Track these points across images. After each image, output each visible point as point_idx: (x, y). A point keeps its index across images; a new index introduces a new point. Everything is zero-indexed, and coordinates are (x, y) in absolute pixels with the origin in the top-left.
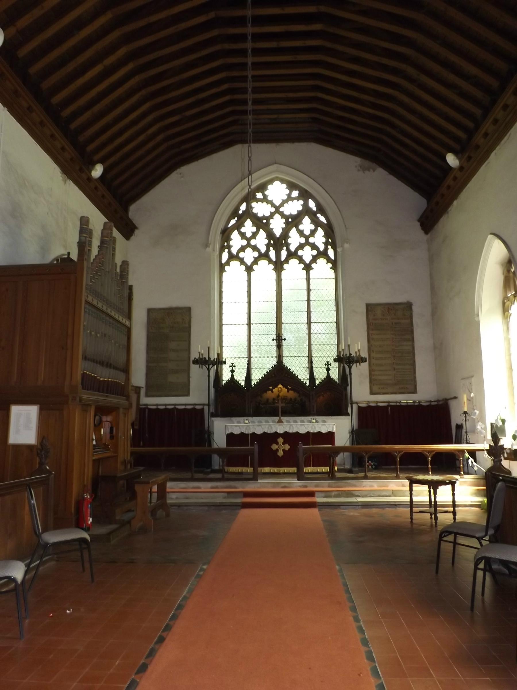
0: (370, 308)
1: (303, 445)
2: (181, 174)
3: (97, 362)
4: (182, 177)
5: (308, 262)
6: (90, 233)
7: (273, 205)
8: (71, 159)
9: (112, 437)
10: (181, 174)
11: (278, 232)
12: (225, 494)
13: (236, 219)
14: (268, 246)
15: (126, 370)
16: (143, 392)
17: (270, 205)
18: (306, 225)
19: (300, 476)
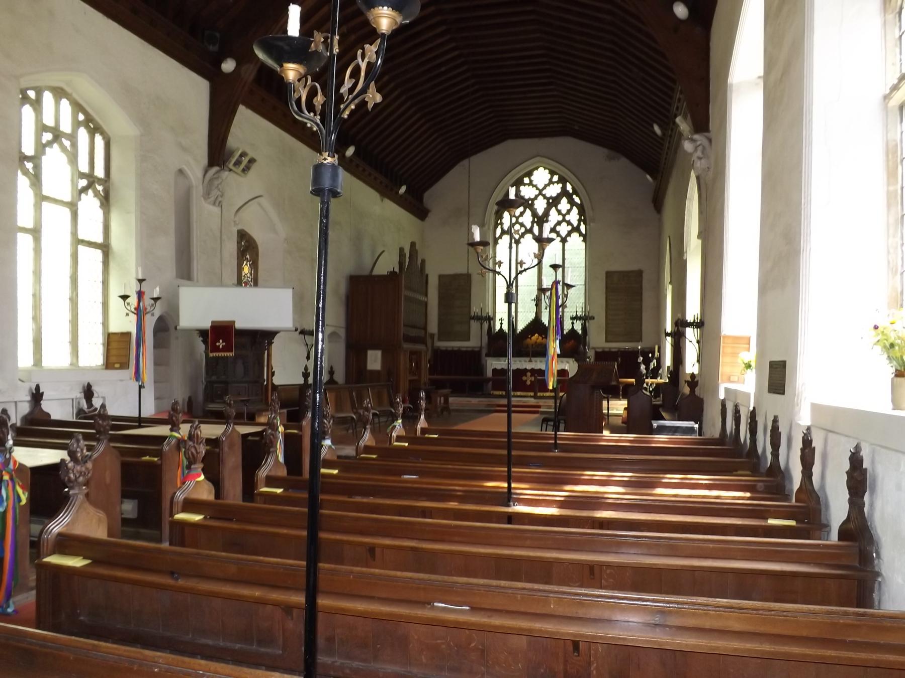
0: (609, 274)
1: (539, 376)
5: (564, 236)
7: (537, 189)
11: (540, 212)
14: (533, 222)
15: (425, 328)
17: (535, 188)
18: (564, 205)
19: (535, 397)
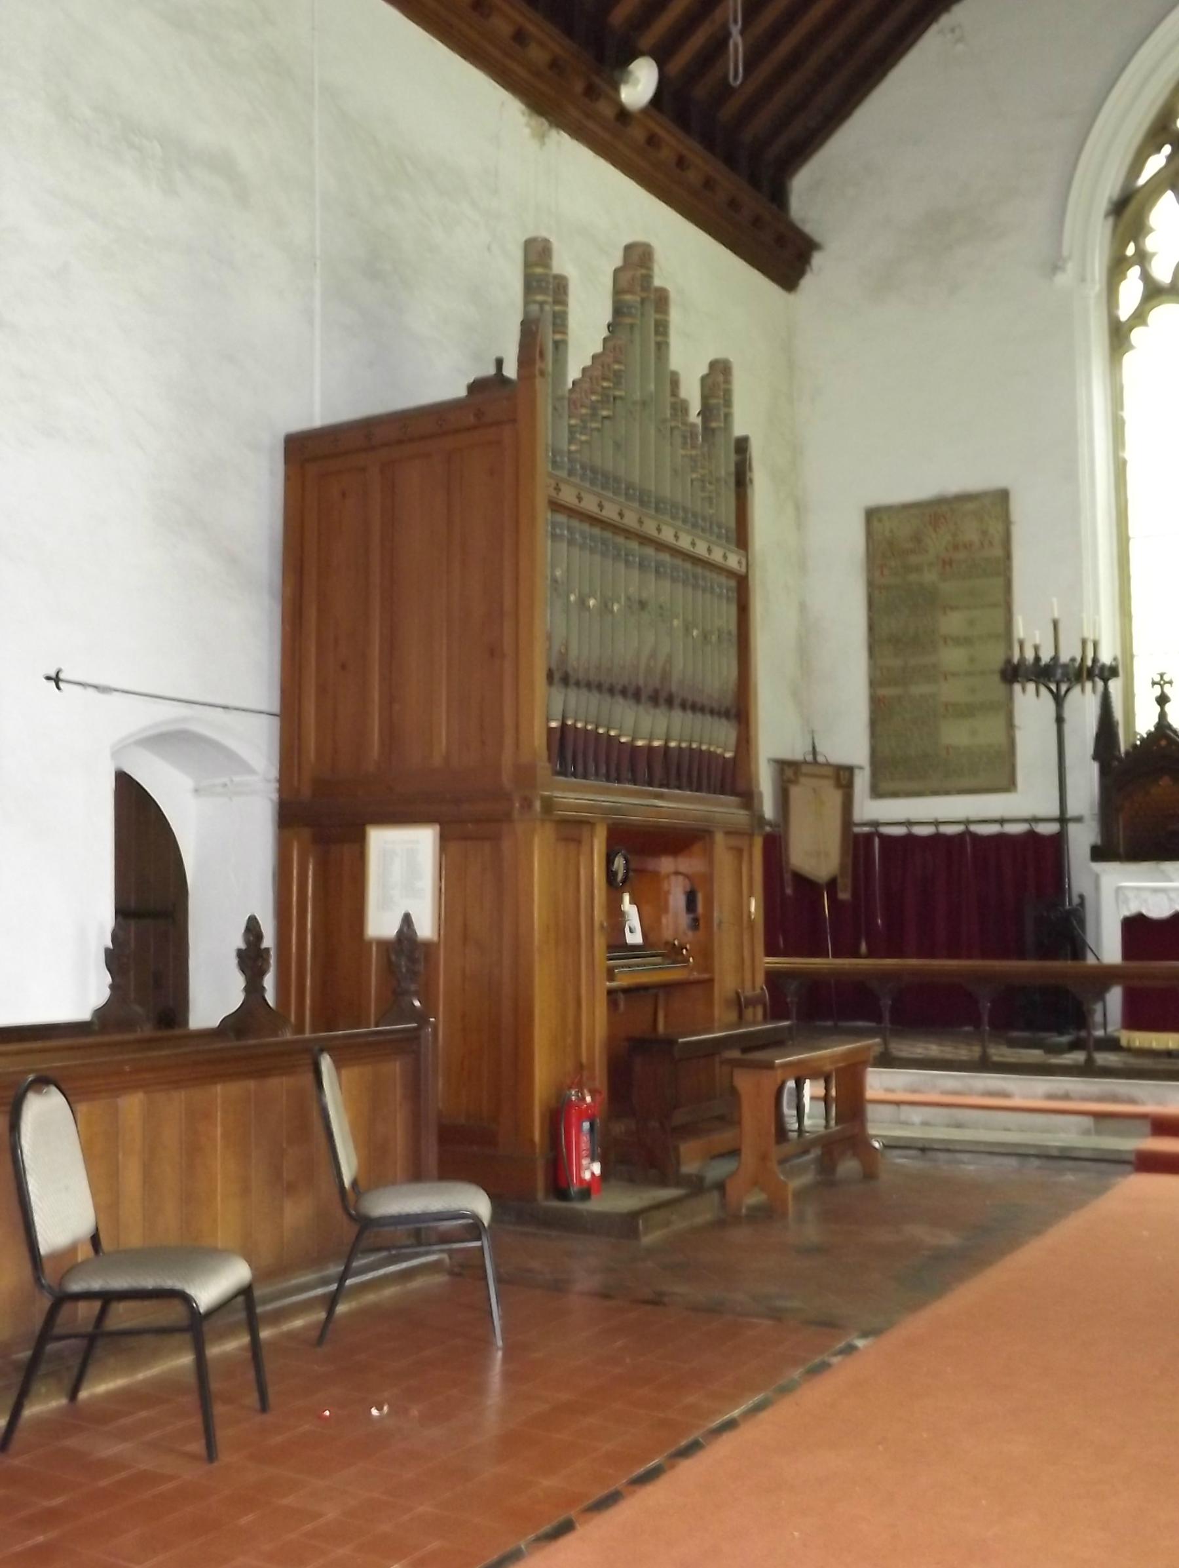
2: (953, 30)
3: (611, 691)
4: (960, 40)
6: (559, 288)
8: (554, 64)
9: (695, 924)
10: (953, 30)
12: (1088, 1122)
13: (1167, 149)
16: (862, 782)
